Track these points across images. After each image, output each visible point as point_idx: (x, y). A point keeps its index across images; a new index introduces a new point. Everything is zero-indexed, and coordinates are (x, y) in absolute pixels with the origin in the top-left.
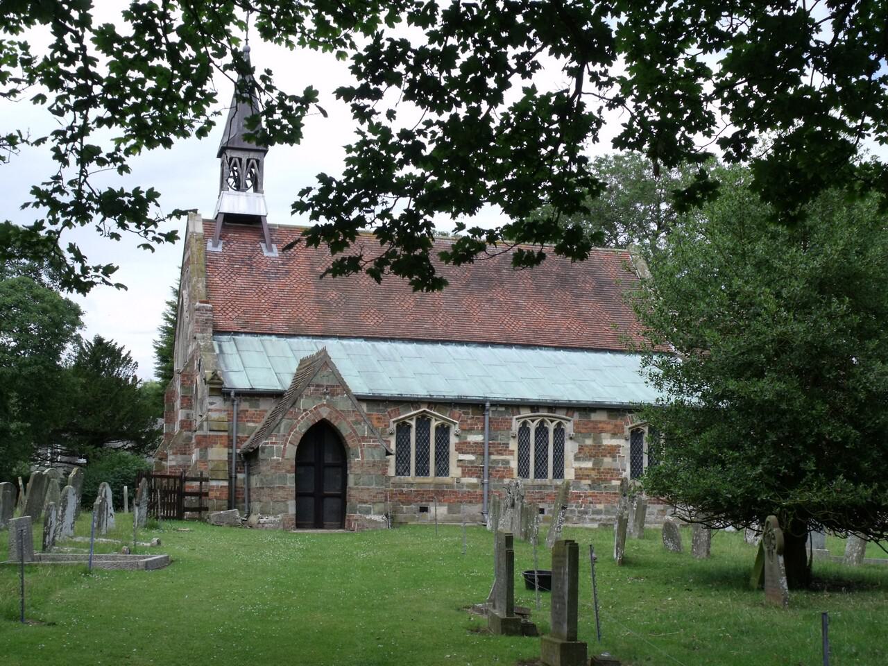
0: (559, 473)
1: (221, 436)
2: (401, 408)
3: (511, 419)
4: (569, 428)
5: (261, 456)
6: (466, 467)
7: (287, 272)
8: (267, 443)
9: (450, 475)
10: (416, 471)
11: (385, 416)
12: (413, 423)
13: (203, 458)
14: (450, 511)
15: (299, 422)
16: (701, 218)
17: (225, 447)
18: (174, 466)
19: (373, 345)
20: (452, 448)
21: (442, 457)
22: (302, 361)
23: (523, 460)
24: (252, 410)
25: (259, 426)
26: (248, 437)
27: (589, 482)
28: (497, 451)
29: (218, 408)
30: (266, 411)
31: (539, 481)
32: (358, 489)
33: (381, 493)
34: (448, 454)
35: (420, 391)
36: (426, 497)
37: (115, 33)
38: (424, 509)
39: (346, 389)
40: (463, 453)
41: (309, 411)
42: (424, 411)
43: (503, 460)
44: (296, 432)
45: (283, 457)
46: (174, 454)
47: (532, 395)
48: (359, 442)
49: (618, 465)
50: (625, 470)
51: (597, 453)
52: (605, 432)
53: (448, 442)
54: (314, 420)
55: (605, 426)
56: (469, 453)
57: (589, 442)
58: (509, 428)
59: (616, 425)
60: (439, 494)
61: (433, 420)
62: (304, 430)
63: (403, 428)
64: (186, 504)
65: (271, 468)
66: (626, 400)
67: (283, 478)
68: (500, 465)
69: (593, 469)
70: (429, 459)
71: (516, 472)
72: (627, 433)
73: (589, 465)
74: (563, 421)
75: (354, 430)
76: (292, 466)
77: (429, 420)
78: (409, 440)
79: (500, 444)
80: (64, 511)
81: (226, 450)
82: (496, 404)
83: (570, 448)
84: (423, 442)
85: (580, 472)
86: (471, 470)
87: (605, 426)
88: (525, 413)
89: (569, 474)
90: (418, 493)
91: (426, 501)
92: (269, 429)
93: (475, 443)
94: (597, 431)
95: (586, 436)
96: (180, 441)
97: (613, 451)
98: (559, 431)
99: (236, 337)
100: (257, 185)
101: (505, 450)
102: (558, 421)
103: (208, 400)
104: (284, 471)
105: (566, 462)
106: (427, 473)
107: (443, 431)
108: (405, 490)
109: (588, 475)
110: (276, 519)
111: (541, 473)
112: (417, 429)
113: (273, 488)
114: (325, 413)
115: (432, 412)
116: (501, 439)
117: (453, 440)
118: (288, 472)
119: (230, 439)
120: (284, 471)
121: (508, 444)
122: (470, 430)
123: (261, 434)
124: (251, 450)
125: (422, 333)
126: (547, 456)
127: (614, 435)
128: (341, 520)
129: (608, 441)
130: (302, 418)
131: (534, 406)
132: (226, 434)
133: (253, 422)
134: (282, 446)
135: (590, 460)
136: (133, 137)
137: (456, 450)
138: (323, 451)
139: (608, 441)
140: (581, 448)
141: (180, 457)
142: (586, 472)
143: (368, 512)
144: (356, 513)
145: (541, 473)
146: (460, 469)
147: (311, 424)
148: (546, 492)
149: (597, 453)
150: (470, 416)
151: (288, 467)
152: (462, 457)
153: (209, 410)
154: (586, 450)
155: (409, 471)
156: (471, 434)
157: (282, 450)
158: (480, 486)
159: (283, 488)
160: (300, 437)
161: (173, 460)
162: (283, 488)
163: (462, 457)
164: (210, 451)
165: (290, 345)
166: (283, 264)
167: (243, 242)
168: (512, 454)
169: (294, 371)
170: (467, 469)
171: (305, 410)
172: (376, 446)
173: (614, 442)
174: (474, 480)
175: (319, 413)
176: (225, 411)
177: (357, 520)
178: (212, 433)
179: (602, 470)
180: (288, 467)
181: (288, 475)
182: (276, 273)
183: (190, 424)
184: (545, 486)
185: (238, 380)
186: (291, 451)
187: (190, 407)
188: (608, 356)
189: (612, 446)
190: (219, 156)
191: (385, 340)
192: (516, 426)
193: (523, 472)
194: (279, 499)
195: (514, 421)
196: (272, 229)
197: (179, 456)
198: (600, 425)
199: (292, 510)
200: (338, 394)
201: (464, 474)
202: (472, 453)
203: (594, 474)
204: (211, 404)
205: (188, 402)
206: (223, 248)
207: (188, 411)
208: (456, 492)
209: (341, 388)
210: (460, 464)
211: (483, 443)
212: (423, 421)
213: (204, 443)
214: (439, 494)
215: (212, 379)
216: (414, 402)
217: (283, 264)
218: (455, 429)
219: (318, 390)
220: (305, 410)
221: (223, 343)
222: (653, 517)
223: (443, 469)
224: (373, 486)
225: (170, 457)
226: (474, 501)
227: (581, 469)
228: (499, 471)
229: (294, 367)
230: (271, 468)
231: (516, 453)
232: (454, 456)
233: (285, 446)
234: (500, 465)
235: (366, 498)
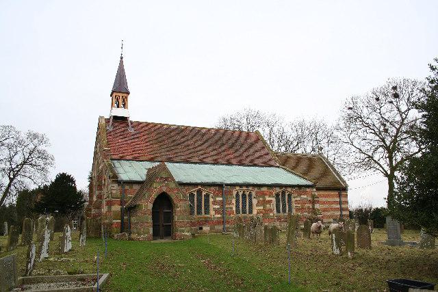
0: (251, 212)
4: (254, 194)
12: (195, 193)
13: (109, 210)
20: (211, 204)
23: (237, 206)
38: (201, 228)
39: (174, 180)
41: (157, 188)
47: (240, 181)
51: (265, 203)
60: (206, 221)
63: (192, 195)
66: (262, 183)
81: (120, 207)
82: (227, 185)
83: (255, 201)
84: (244, 203)
88: (238, 188)
89: (255, 212)
90: (198, 222)
92: (139, 195)
94: (264, 194)
97: (270, 202)
98: (250, 195)
100: (125, 106)
107: (207, 196)
114: (164, 189)
119: (121, 202)
122: (217, 196)
127: (270, 196)
131: (241, 185)
136: (17, 234)
138: (164, 203)
140: (258, 202)
141: (96, 210)
145: (199, 213)
157: (147, 205)
167: (120, 128)
170: (217, 211)
174: (219, 216)
185: (124, 177)
186: (150, 206)
187: (101, 189)
190: (111, 96)
192: (235, 193)
196: (132, 123)
199: (151, 232)
212: (199, 192)
213: (110, 204)
216: (196, 185)
223: (207, 211)
229: (145, 172)
231: (235, 204)
232: (212, 207)
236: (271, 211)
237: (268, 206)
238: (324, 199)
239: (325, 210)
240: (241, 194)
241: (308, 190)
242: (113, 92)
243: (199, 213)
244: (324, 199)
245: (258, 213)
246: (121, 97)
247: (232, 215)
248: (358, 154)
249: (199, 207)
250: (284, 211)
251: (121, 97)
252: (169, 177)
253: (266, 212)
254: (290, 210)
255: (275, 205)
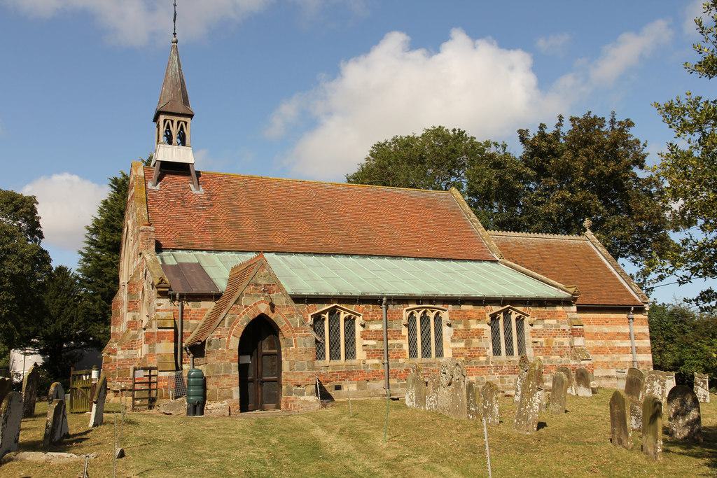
0: (440, 354)
2: (317, 305)
3: (402, 311)
4: (445, 316)
5: (207, 348)
9: (357, 358)
10: (330, 356)
12: (327, 316)
16: (494, 171)
18: (122, 360)
19: (283, 258)
21: (350, 342)
22: (233, 269)
23: (412, 343)
25: (201, 323)
26: (191, 333)
27: (463, 359)
30: (206, 310)
33: (313, 377)
34: (355, 340)
35: (333, 291)
37: (76, 174)
39: (281, 288)
42: (336, 306)
44: (239, 326)
47: (418, 291)
49: (483, 344)
50: (488, 348)
51: (467, 335)
57: (461, 327)
58: (401, 318)
60: (349, 374)
63: (318, 318)
67: (228, 368)
69: (466, 349)
70: (340, 346)
72: (489, 319)
73: (462, 345)
75: (288, 322)
77: (339, 314)
83: (447, 332)
86: (374, 353)
89: (448, 353)
91: (340, 380)
92: (212, 322)
94: (466, 318)
96: (128, 338)
97: (479, 333)
104: (229, 361)
106: (339, 357)
107: (350, 321)
108: (323, 372)
111: (426, 353)
112: (329, 321)
114: (264, 308)
115: (341, 306)
116: (395, 326)
118: (232, 361)
121: (401, 331)
124: (199, 343)
126: (430, 339)
128: (275, 400)
129: (474, 325)
130: (244, 313)
132: (173, 330)
133: (195, 319)
139: (474, 325)
140: (455, 332)
143: (302, 393)
145: (426, 353)
149: (467, 335)
152: (366, 342)
153: (157, 310)
154: (460, 333)
155: (325, 356)
157: (228, 342)
159: (228, 376)
160: (242, 330)
163: (366, 342)
164: (158, 346)
170: (372, 353)
171: (246, 307)
172: (307, 336)
173: (480, 326)
178: (160, 330)
179: (472, 349)
181: (232, 364)
183: (136, 324)
184: (431, 364)
191: (290, 253)
192: (406, 315)
193: (413, 353)
195: (404, 312)
197: (127, 351)
198: (468, 314)
202: (374, 339)
203: (466, 352)
204: (159, 305)
210: (365, 348)
212: (333, 312)
214: (349, 374)
219: (256, 289)
221: (164, 258)
222: (511, 384)
223: (350, 354)
225: (120, 352)
228: (394, 353)
233: (229, 337)
235: (299, 382)
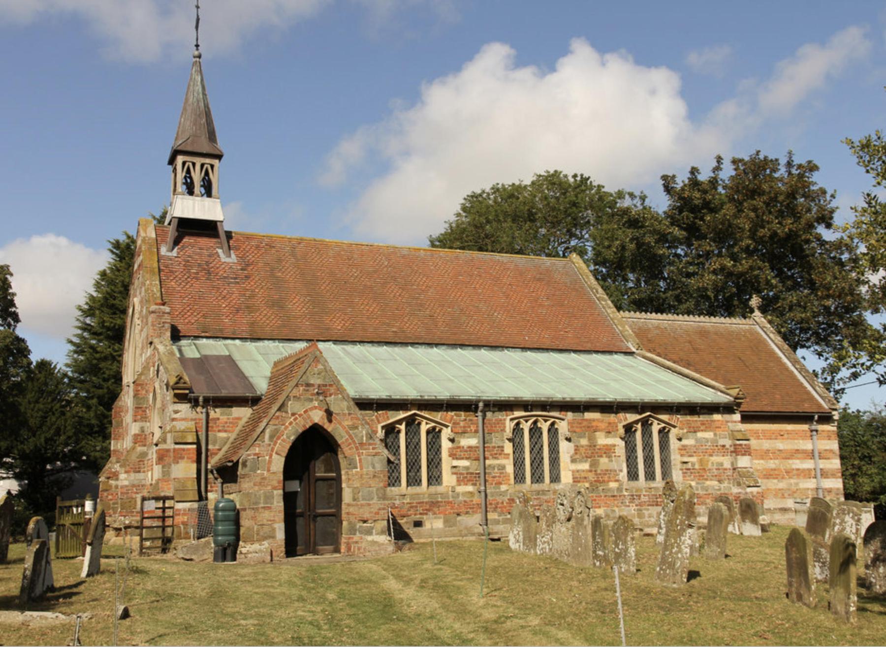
1: (188, 449)
3: (505, 420)
4: (563, 427)
5: (240, 471)
6: (461, 474)
7: (247, 277)
8: (249, 455)
10: (408, 481)
11: (372, 420)
12: (403, 427)
14: (446, 522)
15: (286, 428)
16: (629, 232)
17: (193, 462)
18: (126, 486)
21: (434, 463)
22: (276, 364)
23: (518, 464)
24: (224, 418)
25: (233, 436)
26: (220, 450)
28: (491, 455)
29: (183, 416)
30: (239, 419)
31: (536, 486)
32: (357, 505)
33: (384, 509)
35: (412, 394)
36: (420, 510)
39: (340, 390)
40: (457, 459)
42: (415, 414)
43: (499, 465)
44: (283, 441)
45: (269, 471)
46: (126, 472)
47: (526, 394)
48: (357, 448)
49: (614, 465)
51: (593, 453)
52: (599, 431)
53: (440, 446)
54: (304, 426)
55: (599, 424)
56: (462, 459)
57: (584, 442)
58: (503, 430)
59: (610, 423)
60: (433, 506)
61: (423, 424)
62: (293, 438)
63: (391, 430)
64: (160, 541)
65: (255, 485)
67: (269, 498)
68: (496, 470)
69: (591, 471)
70: (420, 467)
71: (512, 477)
72: (622, 431)
73: (586, 466)
74: (557, 420)
75: (350, 436)
76: (279, 482)
77: (419, 424)
78: (399, 447)
79: (494, 447)
80: (187, 100)
83: (565, 449)
85: (577, 475)
87: (599, 424)
89: (566, 477)
91: (421, 514)
92: (248, 435)
93: (469, 447)
94: (591, 429)
95: (581, 436)
96: (134, 457)
97: (608, 451)
98: (553, 431)
99: (197, 342)
101: (500, 454)
102: (534, 419)
103: (172, 407)
104: (269, 488)
105: (562, 465)
106: (418, 482)
107: (434, 434)
108: (397, 502)
109: (585, 478)
110: (263, 547)
112: (406, 434)
113: (258, 509)
114: (318, 417)
116: (495, 441)
117: (446, 445)
118: (275, 488)
120: (269, 488)
121: (503, 447)
123: (237, 446)
124: (230, 464)
125: (390, 337)
129: (602, 440)
130: (291, 423)
131: (526, 405)
133: (226, 431)
134: (267, 458)
135: (586, 461)
137: (450, 456)
138: (313, 451)
140: (577, 449)
142: (583, 475)
143: (369, 532)
144: (355, 534)
145: (414, 480)
146: (455, 477)
147: (300, 431)
148: (545, 497)
150: (463, 418)
151: (275, 483)
153: (173, 420)
154: (582, 450)
155: (400, 481)
156: (464, 437)
157: (269, 462)
158: (477, 494)
159: (269, 508)
161: (126, 479)
162: (269, 508)
163: (456, 463)
165: (256, 347)
166: (242, 269)
168: (508, 458)
169: (269, 374)
170: (463, 477)
173: (610, 441)
174: (470, 488)
175: (309, 417)
176: (192, 420)
177: (357, 542)
179: (599, 472)
180: (275, 483)
181: (275, 492)
182: (236, 278)
183: (145, 439)
184: (544, 492)
187: (145, 418)
188: (573, 355)
189: (607, 445)
191: (354, 342)
192: (509, 426)
193: (519, 478)
194: (265, 522)
195: (508, 422)
197: (132, 475)
198: (594, 424)
200: (331, 395)
201: (459, 482)
202: (467, 459)
203: (591, 477)
204: (176, 412)
205: (141, 413)
206: (178, 253)
207: (143, 424)
208: (451, 503)
209: (334, 387)
210: (454, 470)
211: (477, 447)
212: (411, 422)
214: (433, 506)
215: (177, 383)
217: (242, 269)
218: (446, 433)
220: (293, 414)
221: (183, 348)
223: (435, 478)
224: (374, 501)
225: (123, 476)
226: (471, 511)
227: (578, 471)
230: (255, 485)
232: (446, 462)
233: (271, 456)
234: (496, 470)
235: (366, 516)
236: (610, 474)
237: (604, 460)
238: (766, 444)
239: (769, 475)
240: (526, 427)
241: (717, 417)
242: (175, 153)
243: (414, 480)
244: (766, 444)
245: (576, 480)
246: (198, 167)
247: (503, 488)
248: (302, 423)
249: (413, 465)
250: (650, 476)
251: (198, 167)
252: (327, 388)
253: (599, 479)
254: (666, 473)
255: (623, 458)
